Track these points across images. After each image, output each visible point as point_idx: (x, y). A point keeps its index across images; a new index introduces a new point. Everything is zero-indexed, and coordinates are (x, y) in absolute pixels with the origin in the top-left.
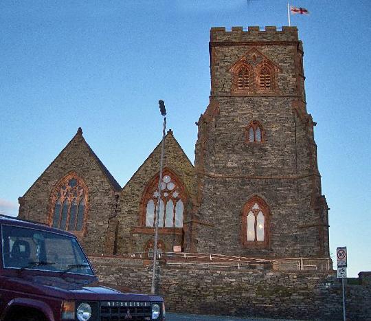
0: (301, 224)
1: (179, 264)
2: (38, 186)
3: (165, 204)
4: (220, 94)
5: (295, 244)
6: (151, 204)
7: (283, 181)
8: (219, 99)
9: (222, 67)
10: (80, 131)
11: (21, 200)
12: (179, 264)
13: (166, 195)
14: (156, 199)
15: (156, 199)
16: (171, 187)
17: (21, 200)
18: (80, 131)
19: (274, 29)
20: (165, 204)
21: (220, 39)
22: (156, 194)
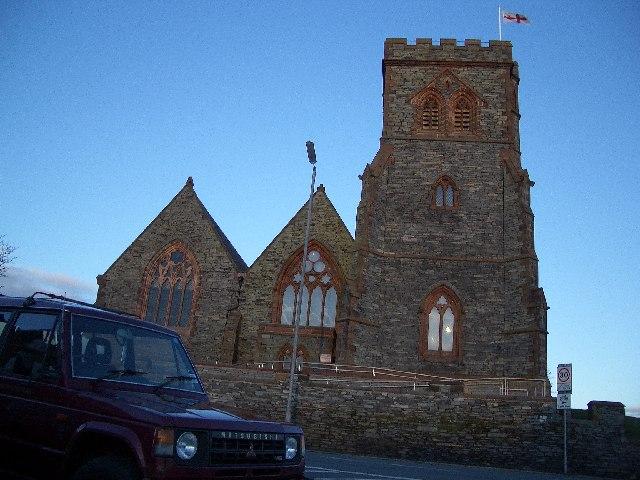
0: (507, 328)
2: (127, 261)
6: (289, 291)
8: (393, 142)
9: (400, 96)
10: (190, 182)
11: (101, 280)
13: (312, 279)
15: (297, 286)
16: (320, 268)
18: (190, 182)
20: (311, 292)
21: (399, 55)
22: (298, 278)
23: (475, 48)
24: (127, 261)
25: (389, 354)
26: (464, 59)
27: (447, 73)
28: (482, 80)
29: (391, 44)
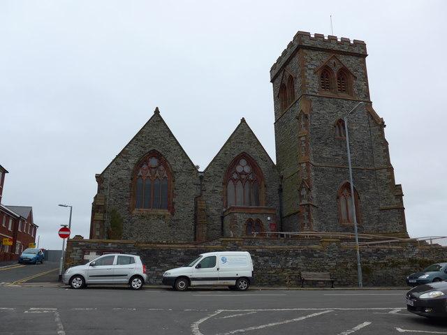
0: (382, 206)
1: (229, 239)
2: (118, 164)
3: (235, 185)
4: (310, 93)
5: (378, 223)
6: (231, 183)
7: (365, 171)
8: (311, 97)
9: (310, 69)
10: (157, 112)
11: (99, 178)
12: (229, 239)
13: (243, 177)
14: (234, 180)
15: (234, 180)
16: (247, 169)
17: (99, 178)
18: (157, 112)
19: (322, 36)
20: (235, 185)
21: (307, 43)
22: (235, 176)
23: (347, 43)
24: (118, 164)
25: (325, 223)
26: (342, 50)
27: (334, 57)
28: (349, 62)
29: (357, 51)
